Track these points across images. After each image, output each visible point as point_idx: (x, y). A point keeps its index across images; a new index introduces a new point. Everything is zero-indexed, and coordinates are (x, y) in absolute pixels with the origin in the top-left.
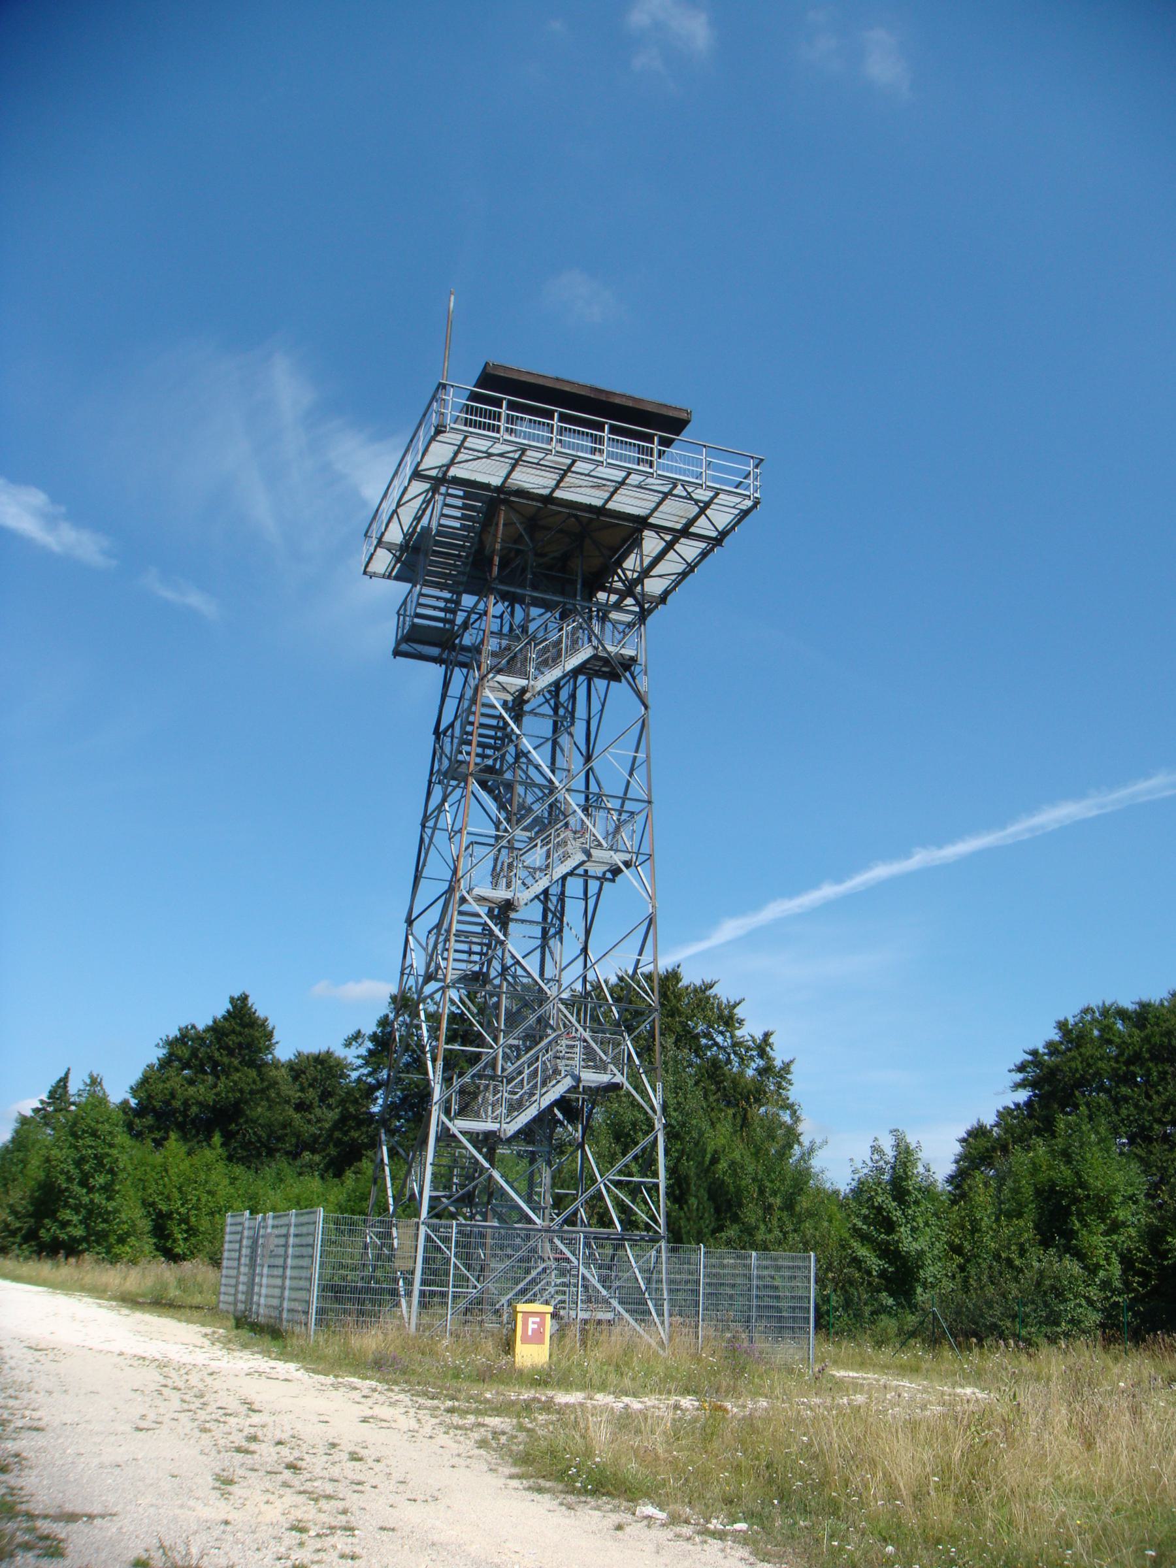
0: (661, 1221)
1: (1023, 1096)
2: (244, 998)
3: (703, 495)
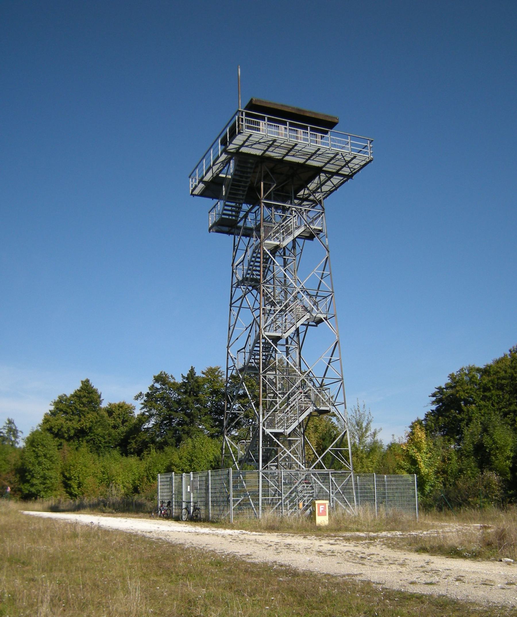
0: (351, 467)
1: (434, 407)
2: (88, 381)
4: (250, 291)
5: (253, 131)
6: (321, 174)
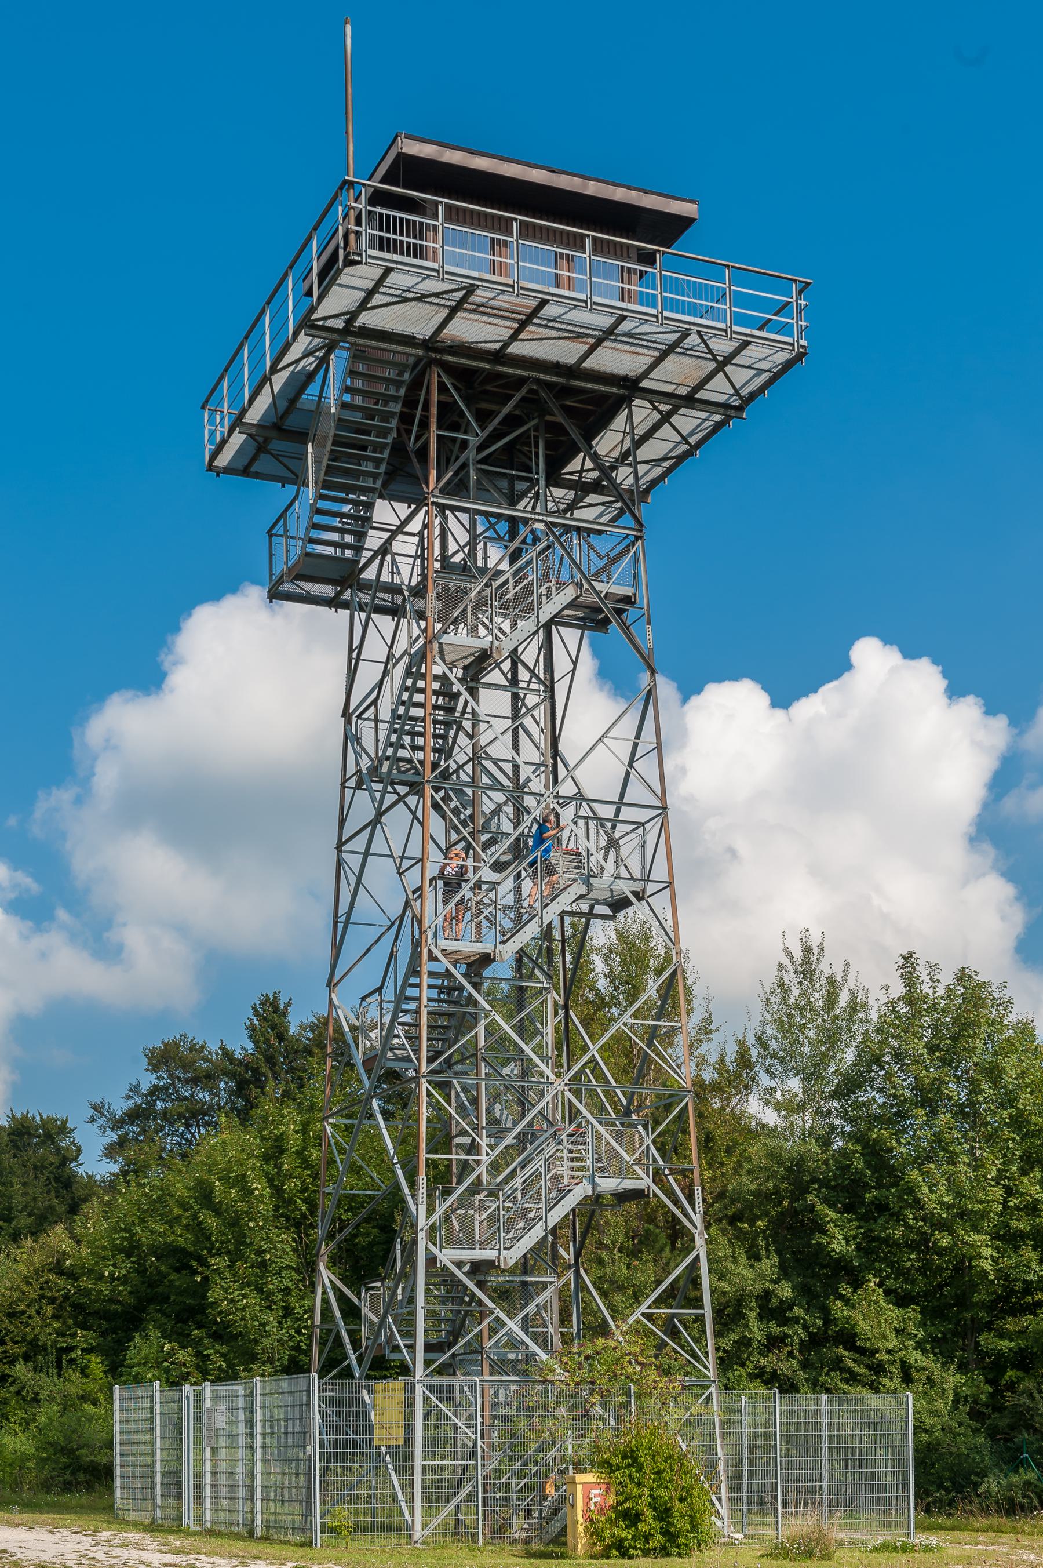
3: (722, 346)
4: (401, 799)
5: (397, 257)
6: (637, 402)
